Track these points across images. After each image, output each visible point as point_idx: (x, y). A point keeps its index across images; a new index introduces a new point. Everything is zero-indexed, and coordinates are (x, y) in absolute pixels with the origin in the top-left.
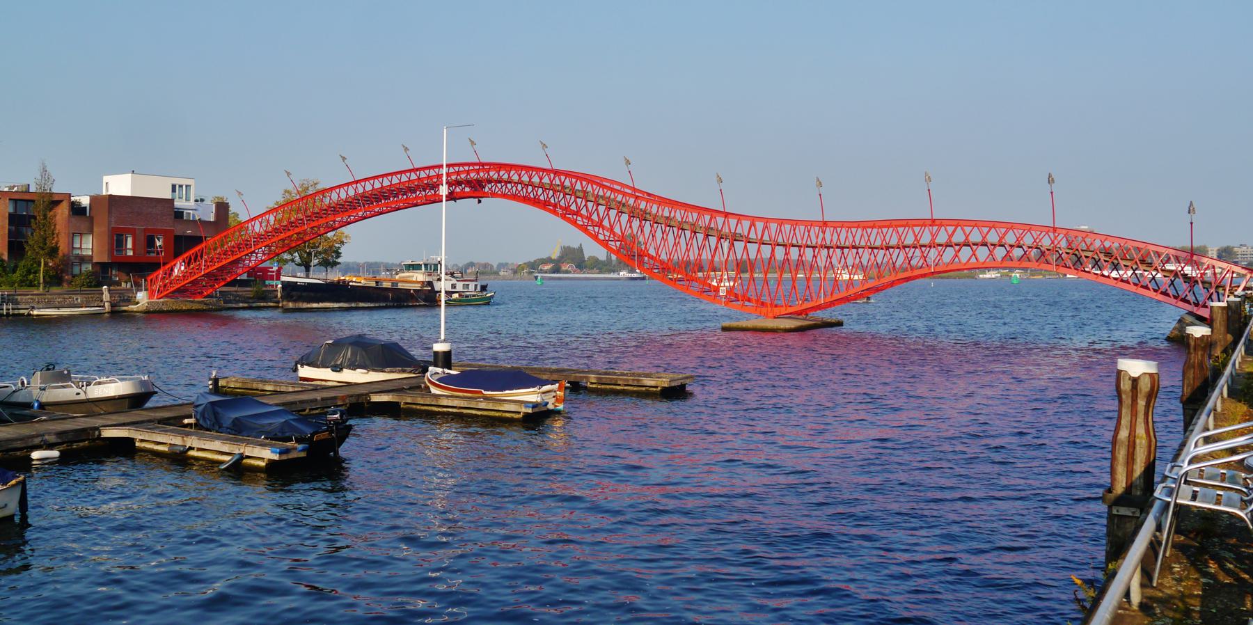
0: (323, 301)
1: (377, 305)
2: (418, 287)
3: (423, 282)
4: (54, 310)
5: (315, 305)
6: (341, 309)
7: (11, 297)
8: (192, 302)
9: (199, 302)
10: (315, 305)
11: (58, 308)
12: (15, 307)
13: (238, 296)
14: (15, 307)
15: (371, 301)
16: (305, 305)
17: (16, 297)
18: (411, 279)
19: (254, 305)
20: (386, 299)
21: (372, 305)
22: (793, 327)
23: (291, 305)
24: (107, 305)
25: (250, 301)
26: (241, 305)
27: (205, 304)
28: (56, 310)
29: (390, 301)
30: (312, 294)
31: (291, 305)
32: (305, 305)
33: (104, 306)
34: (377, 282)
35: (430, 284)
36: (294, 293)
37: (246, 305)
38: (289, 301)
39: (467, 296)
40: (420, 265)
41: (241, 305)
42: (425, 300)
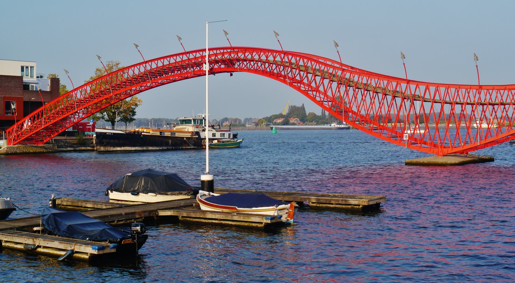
0: (124, 146)
1: (161, 148)
2: (189, 135)
3: (192, 132)
5: (119, 149)
6: (136, 151)
8: (36, 147)
9: (41, 147)
10: (119, 149)
13: (67, 142)
16: (112, 149)
18: (184, 130)
19: (78, 149)
20: (167, 144)
21: (158, 148)
22: (457, 162)
23: (102, 149)
25: (75, 146)
26: (69, 149)
27: (45, 148)
29: (170, 146)
30: (117, 141)
31: (102, 149)
32: (112, 149)
35: (197, 133)
36: (104, 140)
37: (72, 149)
39: (223, 142)
40: (190, 120)
41: (69, 149)
42: (194, 145)
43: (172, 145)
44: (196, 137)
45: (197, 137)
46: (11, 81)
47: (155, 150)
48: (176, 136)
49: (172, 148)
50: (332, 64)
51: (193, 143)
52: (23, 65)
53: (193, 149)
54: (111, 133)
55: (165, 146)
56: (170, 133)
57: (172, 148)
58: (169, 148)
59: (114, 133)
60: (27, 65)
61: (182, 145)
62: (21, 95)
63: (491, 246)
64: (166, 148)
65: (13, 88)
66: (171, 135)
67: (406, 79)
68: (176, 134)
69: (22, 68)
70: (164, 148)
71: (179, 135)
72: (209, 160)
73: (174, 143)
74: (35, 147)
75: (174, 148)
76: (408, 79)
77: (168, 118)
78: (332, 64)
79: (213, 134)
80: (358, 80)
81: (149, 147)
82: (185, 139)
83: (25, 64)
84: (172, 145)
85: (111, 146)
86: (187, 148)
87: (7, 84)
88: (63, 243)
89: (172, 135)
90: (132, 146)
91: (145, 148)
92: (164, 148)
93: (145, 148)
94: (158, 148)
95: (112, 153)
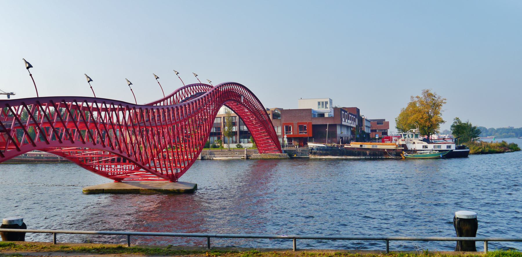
4: (225, 158)
5: (324, 157)
7: (212, 153)
8: (274, 155)
11: (227, 157)
15: (355, 155)
17: (214, 152)
20: (365, 154)
24: (245, 156)
30: (321, 152)
33: (244, 156)
34: (360, 145)
38: (312, 155)
43: (370, 155)
44: (402, 148)
45: (403, 148)
46: (302, 113)
47: (353, 159)
48: (378, 148)
49: (371, 158)
50: (118, 131)
51: (395, 153)
53: (370, 159)
54: (317, 146)
55: (364, 156)
56: (371, 146)
57: (371, 158)
60: (323, 101)
61: (381, 155)
62: (310, 121)
63: (515, 247)
64: (364, 158)
65: (304, 117)
66: (372, 147)
68: (378, 146)
69: (319, 103)
70: (362, 157)
71: (381, 147)
73: (372, 153)
74: (273, 155)
75: (372, 158)
77: (517, 128)
78: (118, 131)
83: (321, 100)
84: (370, 155)
85: (318, 155)
86: (388, 157)
88: (447, 249)
89: (374, 147)
93: (344, 157)
94: (356, 157)
95: (351, 160)
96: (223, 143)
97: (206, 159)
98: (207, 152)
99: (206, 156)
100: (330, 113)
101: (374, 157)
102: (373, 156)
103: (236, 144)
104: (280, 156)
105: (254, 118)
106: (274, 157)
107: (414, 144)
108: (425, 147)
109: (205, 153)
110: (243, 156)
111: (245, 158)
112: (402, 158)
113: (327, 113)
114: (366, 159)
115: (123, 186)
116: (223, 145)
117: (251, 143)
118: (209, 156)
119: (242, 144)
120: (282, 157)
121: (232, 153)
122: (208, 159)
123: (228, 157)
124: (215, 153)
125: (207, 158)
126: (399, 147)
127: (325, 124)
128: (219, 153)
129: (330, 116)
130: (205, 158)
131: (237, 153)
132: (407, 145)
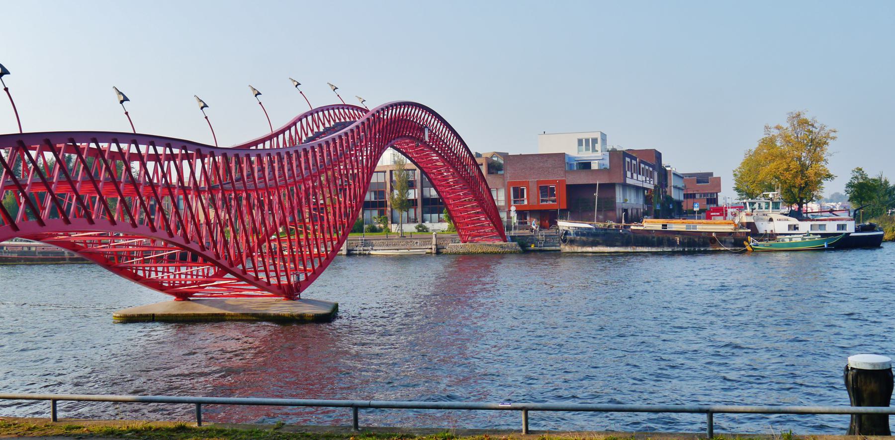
5: (590, 249)
7: (368, 242)
9: (496, 246)
11: (398, 250)
12: (365, 248)
14: (365, 248)
15: (652, 245)
20: (672, 243)
24: (434, 247)
28: (396, 251)
29: (678, 246)
30: (584, 238)
33: (431, 249)
34: (663, 225)
38: (566, 245)
43: (682, 244)
44: (746, 231)
45: (749, 230)
46: (547, 161)
48: (698, 230)
51: (733, 241)
52: (580, 137)
53: (683, 253)
55: (669, 246)
56: (685, 226)
58: (676, 249)
59: (578, 228)
60: (587, 137)
61: (705, 244)
64: (670, 250)
67: (133, 132)
70: (666, 249)
71: (705, 229)
72: (268, 397)
73: (686, 241)
74: (488, 245)
75: (686, 250)
76: (23, 132)
79: (789, 225)
80: (637, 189)
81: (638, 248)
82: (714, 235)
83: (584, 136)
86: (717, 249)
87: (542, 164)
90: (608, 245)
91: (629, 249)
92: (666, 249)
93: (629, 249)
94: (654, 250)
96: (390, 222)
97: (356, 254)
98: (359, 240)
99: (355, 249)
100: (601, 162)
101: (689, 248)
102: (688, 247)
103: (416, 225)
104: (502, 247)
105: (450, 172)
106: (490, 250)
107: (771, 222)
108: (793, 227)
109: (354, 242)
110: (430, 247)
111: (434, 251)
112: (746, 250)
113: (597, 162)
114: (673, 254)
115: (193, 309)
116: (389, 226)
117: (445, 222)
118: (362, 249)
119: (427, 224)
120: (507, 250)
121: (407, 242)
122: (360, 254)
123: (400, 251)
124: (374, 242)
125: (358, 252)
126: (741, 228)
127: (591, 183)
128: (383, 243)
129: (602, 167)
130: (355, 252)
131: (417, 243)
132: (756, 223)
